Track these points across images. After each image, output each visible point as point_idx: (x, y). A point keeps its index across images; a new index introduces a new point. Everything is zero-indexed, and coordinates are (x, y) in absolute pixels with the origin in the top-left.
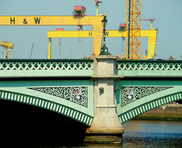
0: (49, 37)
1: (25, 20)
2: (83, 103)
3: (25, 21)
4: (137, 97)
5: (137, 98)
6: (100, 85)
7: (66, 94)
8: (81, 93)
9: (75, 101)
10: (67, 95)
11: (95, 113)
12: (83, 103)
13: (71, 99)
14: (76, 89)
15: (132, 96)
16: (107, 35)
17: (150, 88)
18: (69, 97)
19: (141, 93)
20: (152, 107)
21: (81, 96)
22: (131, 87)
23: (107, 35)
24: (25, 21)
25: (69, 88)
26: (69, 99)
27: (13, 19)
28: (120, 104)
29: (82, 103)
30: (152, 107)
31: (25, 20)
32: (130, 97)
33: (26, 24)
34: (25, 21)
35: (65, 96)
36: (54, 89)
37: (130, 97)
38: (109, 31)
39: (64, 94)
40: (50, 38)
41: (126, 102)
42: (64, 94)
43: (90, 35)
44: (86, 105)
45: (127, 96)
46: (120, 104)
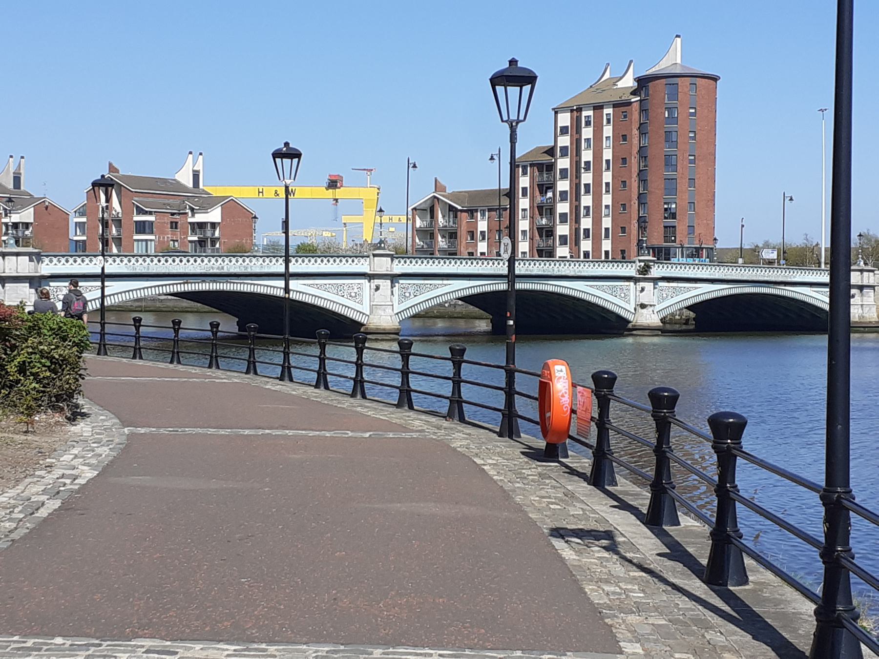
0: (344, 222)
1: (400, 218)
2: (358, 300)
3: (400, 220)
4: (415, 294)
5: (415, 296)
6: (377, 282)
7: (341, 290)
8: (356, 290)
9: (350, 298)
10: (342, 292)
11: (371, 312)
12: (358, 300)
13: (345, 296)
14: (351, 286)
15: (410, 293)
16: (292, 194)
17: (429, 285)
18: (343, 294)
19: (419, 290)
20: (404, 318)
21: (356, 293)
22: (409, 284)
23: (292, 194)
24: (400, 220)
25: (344, 284)
26: (343, 296)
27: (261, 191)
28: (80, 379)
29: (357, 301)
30: (404, 318)
31: (400, 218)
32: (407, 295)
33: (278, 197)
34: (276, 193)
35: (340, 293)
36: (328, 285)
37: (407, 295)
38: (296, 188)
39: (339, 290)
40: (345, 224)
41: (403, 300)
42: (339, 290)
43: (261, 194)
44: (361, 303)
45: (405, 293)
46: (80, 379)
